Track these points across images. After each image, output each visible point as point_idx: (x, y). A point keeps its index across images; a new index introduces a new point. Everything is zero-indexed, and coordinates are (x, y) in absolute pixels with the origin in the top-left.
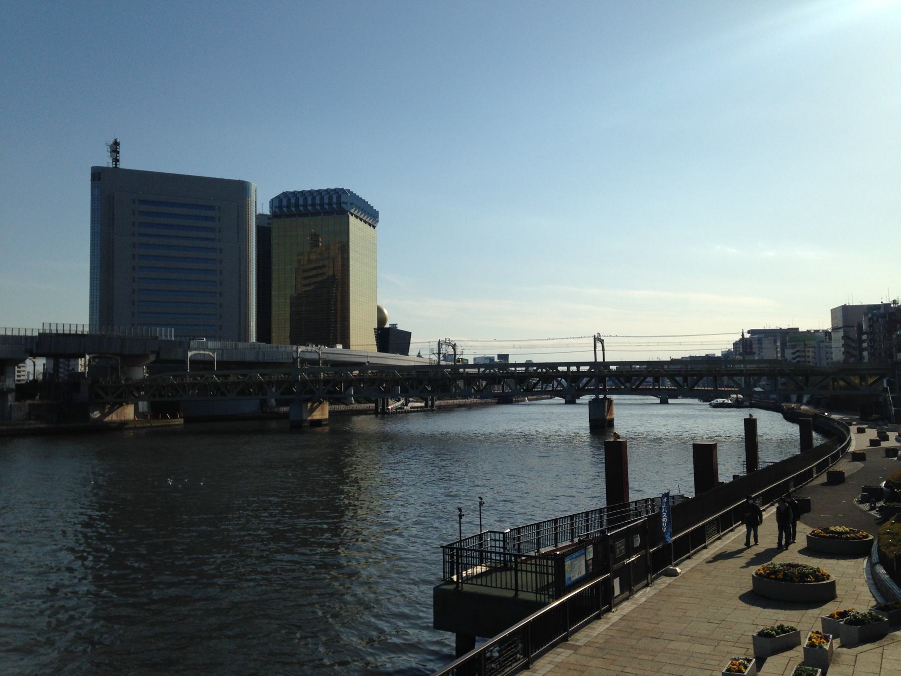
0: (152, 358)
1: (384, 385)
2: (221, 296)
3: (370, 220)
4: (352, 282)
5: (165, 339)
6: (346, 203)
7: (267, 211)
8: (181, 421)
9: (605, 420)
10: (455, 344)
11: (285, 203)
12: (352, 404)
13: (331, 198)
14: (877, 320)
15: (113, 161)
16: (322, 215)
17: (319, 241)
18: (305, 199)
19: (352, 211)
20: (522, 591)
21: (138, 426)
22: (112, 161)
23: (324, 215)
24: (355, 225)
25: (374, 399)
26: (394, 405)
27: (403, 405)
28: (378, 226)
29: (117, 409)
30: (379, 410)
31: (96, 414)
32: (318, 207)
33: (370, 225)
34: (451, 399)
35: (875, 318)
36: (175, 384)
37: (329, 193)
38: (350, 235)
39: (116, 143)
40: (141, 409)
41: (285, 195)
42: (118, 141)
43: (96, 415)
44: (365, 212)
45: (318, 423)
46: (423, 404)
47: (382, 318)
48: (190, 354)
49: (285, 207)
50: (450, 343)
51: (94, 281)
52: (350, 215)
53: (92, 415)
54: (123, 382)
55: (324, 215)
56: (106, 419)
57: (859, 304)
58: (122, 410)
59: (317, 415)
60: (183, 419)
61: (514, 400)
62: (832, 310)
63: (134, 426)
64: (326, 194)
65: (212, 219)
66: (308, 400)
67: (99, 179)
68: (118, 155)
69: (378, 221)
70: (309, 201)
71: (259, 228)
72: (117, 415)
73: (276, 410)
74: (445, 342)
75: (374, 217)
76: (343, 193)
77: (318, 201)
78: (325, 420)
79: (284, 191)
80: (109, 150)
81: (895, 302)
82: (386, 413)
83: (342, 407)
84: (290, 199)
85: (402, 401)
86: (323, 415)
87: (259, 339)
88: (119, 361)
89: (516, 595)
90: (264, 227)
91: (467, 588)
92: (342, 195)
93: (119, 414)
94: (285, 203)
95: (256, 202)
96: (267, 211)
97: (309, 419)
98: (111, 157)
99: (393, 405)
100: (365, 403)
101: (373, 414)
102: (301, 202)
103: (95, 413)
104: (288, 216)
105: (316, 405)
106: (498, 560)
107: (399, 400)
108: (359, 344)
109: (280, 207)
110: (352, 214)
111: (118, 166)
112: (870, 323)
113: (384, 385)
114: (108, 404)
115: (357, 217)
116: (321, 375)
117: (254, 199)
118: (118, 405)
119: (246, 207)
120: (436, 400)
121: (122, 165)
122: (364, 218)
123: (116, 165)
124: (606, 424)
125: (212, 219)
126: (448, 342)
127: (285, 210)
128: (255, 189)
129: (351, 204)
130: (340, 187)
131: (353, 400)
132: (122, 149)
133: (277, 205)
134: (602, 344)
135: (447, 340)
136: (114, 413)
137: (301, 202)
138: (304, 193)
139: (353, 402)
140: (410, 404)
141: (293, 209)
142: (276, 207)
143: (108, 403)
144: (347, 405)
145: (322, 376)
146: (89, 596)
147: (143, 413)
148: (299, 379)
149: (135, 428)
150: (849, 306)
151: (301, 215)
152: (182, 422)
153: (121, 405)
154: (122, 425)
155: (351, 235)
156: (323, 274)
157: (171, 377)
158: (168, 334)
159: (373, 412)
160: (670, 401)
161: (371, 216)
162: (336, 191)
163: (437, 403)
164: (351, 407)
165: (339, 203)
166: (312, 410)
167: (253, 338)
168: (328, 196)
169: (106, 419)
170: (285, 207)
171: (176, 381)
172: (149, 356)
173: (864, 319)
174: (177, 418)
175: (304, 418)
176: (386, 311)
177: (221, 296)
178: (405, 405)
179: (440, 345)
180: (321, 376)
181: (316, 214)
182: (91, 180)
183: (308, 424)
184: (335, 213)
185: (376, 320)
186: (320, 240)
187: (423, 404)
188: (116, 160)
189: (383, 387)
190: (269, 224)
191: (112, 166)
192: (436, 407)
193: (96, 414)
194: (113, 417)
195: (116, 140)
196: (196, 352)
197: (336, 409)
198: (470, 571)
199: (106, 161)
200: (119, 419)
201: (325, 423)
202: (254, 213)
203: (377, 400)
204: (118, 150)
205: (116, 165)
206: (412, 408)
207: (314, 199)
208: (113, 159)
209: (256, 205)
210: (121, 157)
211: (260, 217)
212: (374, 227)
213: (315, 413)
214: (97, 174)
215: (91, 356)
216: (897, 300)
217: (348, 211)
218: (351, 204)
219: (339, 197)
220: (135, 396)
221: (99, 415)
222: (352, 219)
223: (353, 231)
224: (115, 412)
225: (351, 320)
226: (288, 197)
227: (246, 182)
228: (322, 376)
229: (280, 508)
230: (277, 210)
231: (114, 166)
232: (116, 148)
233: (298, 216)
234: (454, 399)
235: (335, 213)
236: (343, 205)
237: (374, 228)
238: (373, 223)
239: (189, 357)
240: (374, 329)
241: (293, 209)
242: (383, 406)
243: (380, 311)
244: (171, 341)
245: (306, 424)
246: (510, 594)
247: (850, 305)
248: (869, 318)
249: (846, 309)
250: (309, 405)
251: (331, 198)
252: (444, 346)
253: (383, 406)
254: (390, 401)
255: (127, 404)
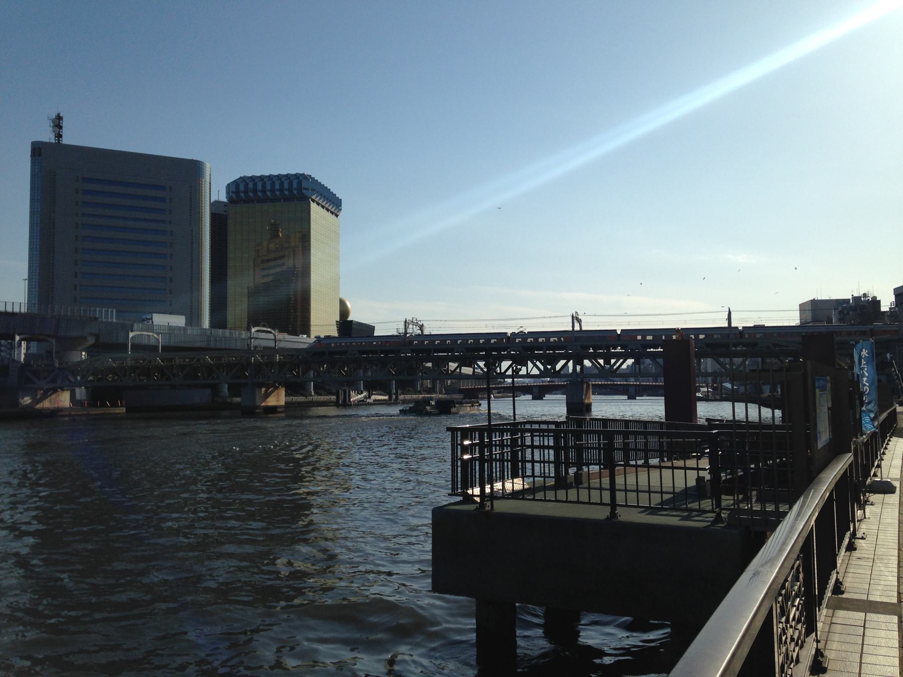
0: (91, 341)
1: (346, 369)
2: (171, 282)
3: (332, 208)
4: (314, 266)
5: (106, 320)
6: (307, 189)
7: (223, 198)
8: (124, 410)
9: (583, 403)
10: (423, 324)
11: (242, 188)
12: (311, 395)
13: (291, 183)
14: (848, 312)
15: (55, 137)
16: (282, 201)
17: (279, 230)
18: (264, 185)
19: (314, 197)
20: (626, 506)
21: (73, 413)
22: (54, 137)
23: (284, 201)
24: (316, 211)
25: (334, 391)
26: (357, 398)
27: (365, 397)
28: (341, 214)
29: (51, 395)
30: (340, 402)
31: (27, 400)
32: (278, 193)
33: (332, 213)
34: (415, 394)
35: (846, 312)
36: (114, 367)
37: (289, 178)
38: (312, 222)
39: (59, 118)
40: (78, 397)
41: (243, 179)
42: (61, 115)
43: (26, 401)
44: (331, 201)
45: (273, 410)
46: (386, 398)
47: (344, 312)
48: (131, 335)
49: (242, 192)
50: (417, 323)
51: (33, 263)
52: (311, 202)
53: (21, 401)
54: (57, 365)
55: (284, 201)
56: (39, 406)
57: (828, 298)
58: (56, 397)
59: (272, 401)
60: (125, 408)
61: (480, 396)
62: (800, 305)
63: (68, 413)
64: (286, 179)
65: (162, 200)
66: (260, 386)
67: (40, 155)
68: (61, 130)
69: (341, 210)
70: (268, 187)
71: (213, 216)
72: (51, 401)
73: (229, 400)
74: (412, 322)
75: (337, 205)
76: (303, 179)
77: (277, 187)
78: (281, 407)
79: (242, 176)
80: (52, 125)
81: (865, 295)
82: (348, 405)
83: (301, 399)
84: (248, 184)
85: (365, 394)
86: (278, 401)
87: (213, 325)
88: (54, 344)
89: (613, 514)
90: (220, 215)
91: (500, 506)
92: (303, 180)
93: (52, 401)
94: (242, 188)
95: (210, 184)
96: (223, 198)
97: (263, 404)
98: (54, 132)
99: (355, 397)
100: (325, 395)
101: (334, 406)
102: (259, 187)
103: (26, 399)
104: (246, 202)
105: (270, 390)
106: (557, 455)
107: (362, 393)
108: (318, 324)
109: (237, 192)
110: (313, 201)
111: (61, 142)
112: (840, 316)
113: (346, 369)
114: (40, 390)
115: (318, 204)
116: (276, 356)
117: (208, 180)
118: (51, 391)
119: (199, 185)
120: (400, 395)
121: (66, 140)
122: (327, 206)
123: (59, 140)
124: (584, 408)
125: (162, 200)
126: (416, 322)
127: (242, 195)
128: (209, 173)
129: (313, 190)
130: (301, 172)
131: (313, 392)
132: (65, 124)
133: (234, 190)
134: (580, 324)
135: (415, 319)
136: (47, 400)
137: (259, 187)
138: (262, 178)
139: (313, 394)
140: (374, 397)
141: (251, 194)
142: (232, 192)
143: (41, 389)
144: (306, 397)
145: (278, 357)
146: (197, 631)
147: (80, 400)
148: (253, 361)
149: (70, 415)
150: (818, 301)
151: (259, 201)
152: (124, 411)
153: (55, 391)
154: (55, 413)
155: (312, 222)
156: (283, 264)
157: (110, 360)
158: (112, 316)
159: (333, 404)
160: (637, 398)
161: (333, 204)
162: (297, 176)
163: (401, 397)
164: (310, 399)
165: (300, 188)
166: (267, 395)
167: (206, 324)
168: (288, 181)
169: (39, 406)
170: (242, 192)
171: (115, 364)
172: (88, 339)
173: (833, 313)
174: (118, 406)
175: (257, 404)
176: (348, 304)
177: (171, 282)
178: (368, 398)
179: (407, 324)
180: (276, 359)
181: (275, 200)
182: (31, 156)
183: (262, 411)
184: (295, 200)
185: (339, 312)
186: (280, 230)
187: (386, 398)
188: (59, 136)
189: (345, 371)
190: (225, 211)
191: (54, 142)
192: (401, 400)
193: (27, 400)
194: (46, 404)
195: (58, 115)
196: (139, 333)
197: (294, 400)
198: (498, 486)
199: (48, 136)
200: (53, 406)
201: (280, 410)
202: (208, 200)
203: (339, 391)
204: (61, 125)
205: (59, 140)
206: (375, 400)
207: (273, 184)
208: (55, 134)
209: (210, 186)
210: (65, 132)
211: (215, 205)
212: (337, 216)
213: (269, 399)
214: (38, 150)
215: (22, 337)
216: (867, 293)
217: (310, 197)
218: (313, 190)
219: (300, 183)
220: (70, 381)
221: (30, 401)
222: (313, 206)
223: (315, 218)
224: (49, 398)
225: (312, 311)
226: (246, 181)
227: (199, 161)
228: (278, 357)
229: (219, 486)
230: (234, 196)
231: (57, 141)
232: (59, 123)
233: (256, 202)
234: (419, 394)
235: (295, 200)
236: (304, 191)
237: (337, 217)
238: (335, 212)
239: (130, 337)
240: (337, 321)
241: (251, 194)
242: (345, 398)
243: (342, 303)
244: (112, 322)
245: (259, 411)
246: (602, 513)
247: (819, 299)
248: (839, 311)
249: (814, 302)
250: (263, 390)
251: (291, 183)
252: (411, 326)
253: (345, 398)
254: (352, 393)
255: (63, 390)
